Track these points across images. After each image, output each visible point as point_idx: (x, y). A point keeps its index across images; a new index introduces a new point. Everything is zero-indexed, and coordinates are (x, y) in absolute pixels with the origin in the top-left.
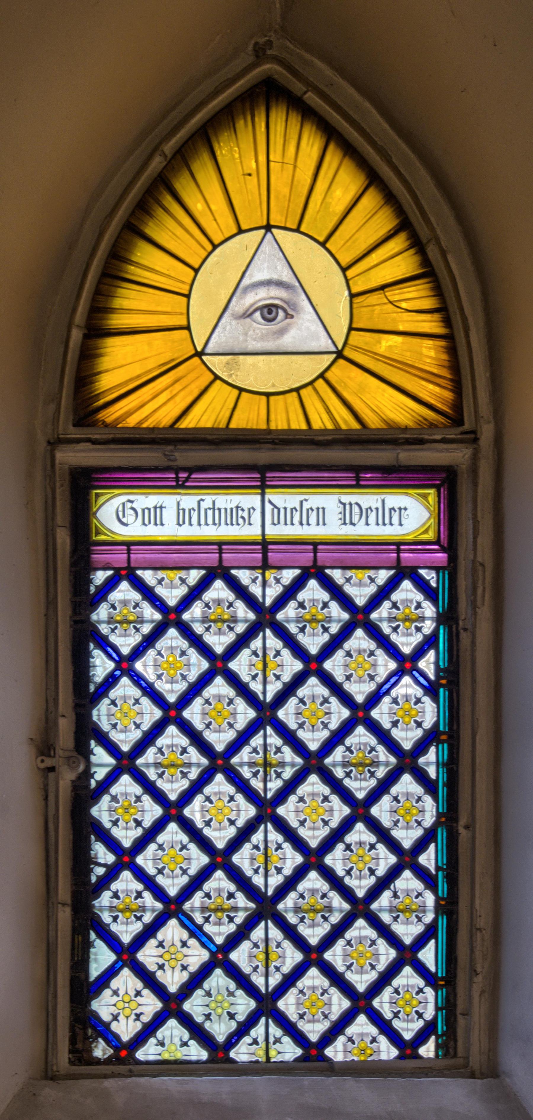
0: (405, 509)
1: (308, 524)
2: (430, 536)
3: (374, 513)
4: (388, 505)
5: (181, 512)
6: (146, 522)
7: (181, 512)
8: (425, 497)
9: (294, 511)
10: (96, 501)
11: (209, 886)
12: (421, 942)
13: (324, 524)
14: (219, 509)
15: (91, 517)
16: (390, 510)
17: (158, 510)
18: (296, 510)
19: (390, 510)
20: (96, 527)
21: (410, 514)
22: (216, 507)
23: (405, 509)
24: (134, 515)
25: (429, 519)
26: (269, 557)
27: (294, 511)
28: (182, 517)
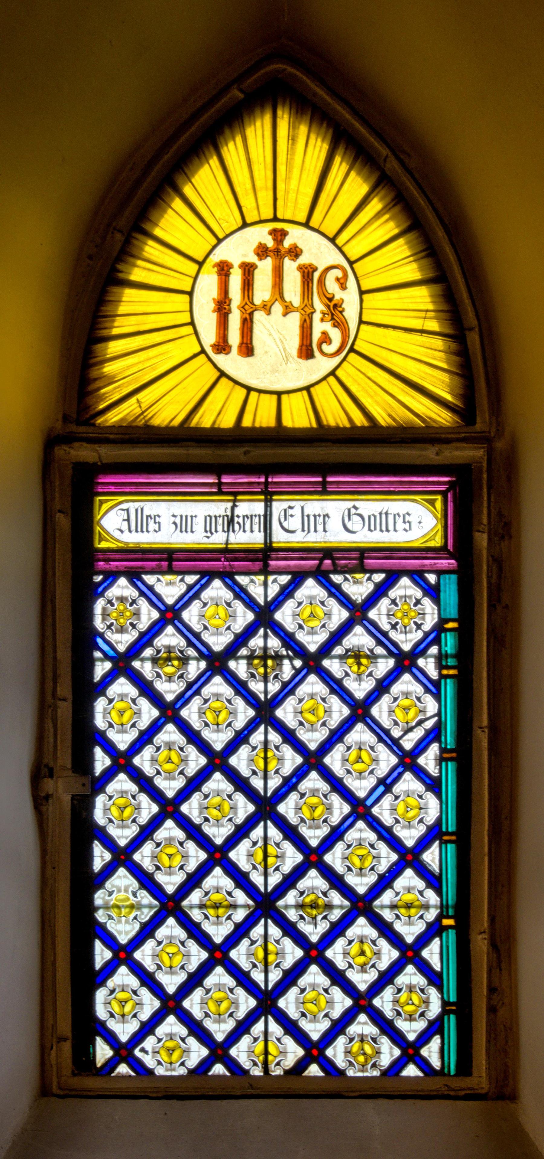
0: (196, 516)
1: (395, 530)
2: (437, 542)
3: (257, 519)
4: (146, 512)
5: (306, 519)
6: (372, 528)
7: (306, 519)
8: (432, 502)
9: (397, 516)
10: (99, 510)
11: (303, 884)
12: (423, 940)
13: (192, 532)
14: (308, 516)
15: (95, 525)
16: (147, 517)
17: (384, 516)
18: (151, 518)
19: (147, 517)
20: (99, 532)
21: (415, 520)
22: (306, 514)
23: (196, 516)
24: (361, 522)
25: (436, 525)
26: (365, 564)
27: (397, 516)
28: (183, 524)
